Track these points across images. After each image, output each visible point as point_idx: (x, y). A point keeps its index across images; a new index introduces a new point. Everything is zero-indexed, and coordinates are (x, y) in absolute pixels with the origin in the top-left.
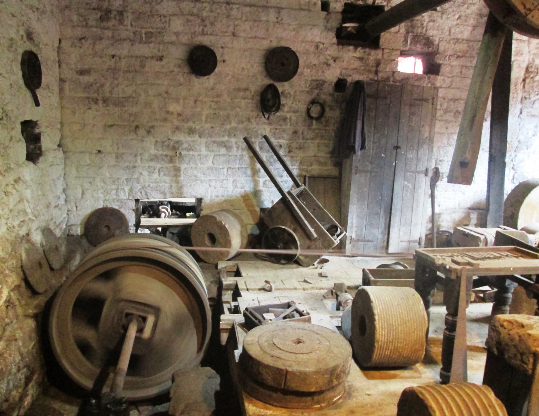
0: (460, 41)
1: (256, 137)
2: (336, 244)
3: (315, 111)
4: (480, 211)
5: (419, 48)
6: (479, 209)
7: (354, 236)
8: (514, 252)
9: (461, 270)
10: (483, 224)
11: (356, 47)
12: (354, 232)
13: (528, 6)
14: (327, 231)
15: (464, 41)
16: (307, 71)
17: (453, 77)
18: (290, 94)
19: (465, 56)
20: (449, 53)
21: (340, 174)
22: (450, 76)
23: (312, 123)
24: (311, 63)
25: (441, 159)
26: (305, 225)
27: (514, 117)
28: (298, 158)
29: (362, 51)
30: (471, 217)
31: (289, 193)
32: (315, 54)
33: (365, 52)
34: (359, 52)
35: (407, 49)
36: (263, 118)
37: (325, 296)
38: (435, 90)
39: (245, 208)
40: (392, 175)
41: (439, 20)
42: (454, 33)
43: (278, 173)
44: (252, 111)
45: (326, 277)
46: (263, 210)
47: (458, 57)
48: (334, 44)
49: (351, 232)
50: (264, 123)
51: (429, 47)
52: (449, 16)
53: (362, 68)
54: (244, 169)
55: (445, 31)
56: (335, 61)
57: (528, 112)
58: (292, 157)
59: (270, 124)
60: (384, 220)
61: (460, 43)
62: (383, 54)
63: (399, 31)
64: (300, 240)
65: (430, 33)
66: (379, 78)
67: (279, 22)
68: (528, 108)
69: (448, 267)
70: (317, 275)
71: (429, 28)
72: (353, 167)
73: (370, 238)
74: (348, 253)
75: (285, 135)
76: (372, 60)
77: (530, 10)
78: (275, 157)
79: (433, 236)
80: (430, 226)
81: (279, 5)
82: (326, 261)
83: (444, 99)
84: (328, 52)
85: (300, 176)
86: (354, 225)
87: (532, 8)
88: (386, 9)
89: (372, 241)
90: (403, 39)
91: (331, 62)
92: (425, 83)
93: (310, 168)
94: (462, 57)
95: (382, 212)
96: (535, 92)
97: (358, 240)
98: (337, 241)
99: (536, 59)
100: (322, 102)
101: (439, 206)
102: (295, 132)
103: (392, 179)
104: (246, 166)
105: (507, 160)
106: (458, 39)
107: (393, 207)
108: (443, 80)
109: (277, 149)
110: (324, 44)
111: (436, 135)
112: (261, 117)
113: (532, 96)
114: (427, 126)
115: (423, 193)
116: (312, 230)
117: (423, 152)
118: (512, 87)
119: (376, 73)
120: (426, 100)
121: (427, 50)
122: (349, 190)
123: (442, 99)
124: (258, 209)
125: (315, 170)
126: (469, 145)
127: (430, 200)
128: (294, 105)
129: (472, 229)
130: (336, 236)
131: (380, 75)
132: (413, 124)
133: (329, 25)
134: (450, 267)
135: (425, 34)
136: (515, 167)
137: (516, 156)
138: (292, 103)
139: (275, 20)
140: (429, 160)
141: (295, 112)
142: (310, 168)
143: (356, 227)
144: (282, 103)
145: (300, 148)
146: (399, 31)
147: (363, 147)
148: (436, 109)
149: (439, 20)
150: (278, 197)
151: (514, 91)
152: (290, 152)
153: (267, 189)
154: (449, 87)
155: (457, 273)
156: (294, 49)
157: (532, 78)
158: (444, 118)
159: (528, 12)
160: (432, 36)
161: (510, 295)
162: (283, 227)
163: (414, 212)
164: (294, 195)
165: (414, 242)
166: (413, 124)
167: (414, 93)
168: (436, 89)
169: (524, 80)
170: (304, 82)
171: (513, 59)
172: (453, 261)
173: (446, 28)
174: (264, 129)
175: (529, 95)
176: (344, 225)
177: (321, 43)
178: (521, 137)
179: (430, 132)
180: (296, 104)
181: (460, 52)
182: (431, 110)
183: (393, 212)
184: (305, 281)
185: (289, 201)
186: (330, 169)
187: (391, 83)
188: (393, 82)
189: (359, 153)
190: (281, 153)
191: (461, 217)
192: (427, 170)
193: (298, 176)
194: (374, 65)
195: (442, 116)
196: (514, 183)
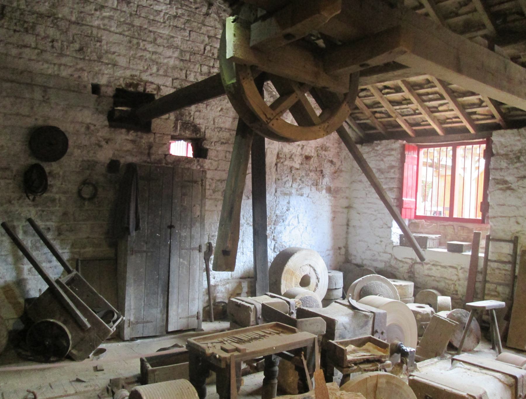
0: (223, 129)
1: (19, 219)
2: (113, 332)
3: (87, 192)
4: (249, 279)
5: (188, 134)
6: (249, 278)
7: (132, 319)
8: (276, 328)
9: (230, 358)
10: (253, 293)
11: (128, 131)
12: (132, 315)
13: (268, 116)
14: (101, 318)
15: (227, 130)
16: (77, 152)
17: (219, 160)
18: (58, 174)
19: (228, 143)
20: (215, 140)
21: (116, 255)
22: (216, 159)
23: (84, 204)
24: (81, 143)
25: (213, 234)
26: (76, 314)
27: (271, 195)
28: (70, 241)
29: (135, 134)
30: (243, 286)
31: (57, 281)
32: (86, 135)
33: (137, 135)
34: (132, 135)
35: (177, 134)
36: (27, 200)
37: (100, 395)
38: (204, 173)
39: (6, 301)
40: (168, 254)
41: (204, 110)
42: (218, 123)
43: (47, 258)
44: (13, 192)
45: (103, 370)
46: (29, 301)
47: (222, 143)
48: (106, 126)
49: (129, 316)
50: (28, 204)
51: (196, 134)
52: (213, 108)
53: (135, 150)
54: (3, 257)
55: (209, 120)
56: (107, 143)
57: (281, 191)
58: (62, 240)
59: (35, 206)
60: (162, 300)
61: (223, 131)
62: (154, 138)
63: (169, 118)
64: (71, 333)
65: (197, 121)
66: (152, 160)
67: (46, 100)
68: (280, 187)
69: (217, 356)
70: (92, 369)
71: (195, 117)
72: (129, 248)
73: (149, 319)
74: (126, 337)
75: (54, 217)
76: (144, 143)
77: (270, 119)
78: (42, 242)
79: (210, 309)
80: (207, 298)
81: (45, 84)
82: (103, 351)
83: (212, 180)
84: (100, 134)
85: (71, 259)
86: (132, 308)
87: (272, 118)
88: (157, 97)
89: (152, 322)
90: (173, 125)
91: (103, 143)
92: (195, 167)
93: (82, 251)
94: (226, 143)
95: (160, 292)
96: (285, 174)
97: (137, 323)
98: (113, 329)
99: (284, 148)
100: (94, 183)
101: (214, 278)
102: (65, 214)
103: (168, 257)
104: (6, 253)
105: (268, 232)
106: (221, 128)
107: (170, 285)
108: (211, 163)
109: (44, 232)
110: (95, 126)
111: (207, 213)
112: (25, 199)
113: (283, 177)
114: (197, 205)
115: (198, 269)
116: (85, 320)
117: (196, 230)
118: (267, 170)
119: (149, 155)
120: (196, 182)
121: (195, 137)
122: (125, 272)
123: (210, 180)
124: (22, 301)
125: (89, 251)
126: (230, 235)
127: (205, 273)
128: (63, 186)
129: (245, 300)
130: (112, 323)
131: (153, 157)
132: (185, 204)
133: (100, 108)
134: (219, 356)
135: (193, 122)
136: (275, 238)
137: (275, 228)
138: (62, 184)
139: (42, 99)
140: (202, 236)
141: (64, 193)
142: (82, 251)
143: (134, 309)
144: (49, 183)
145: (71, 230)
146: (169, 118)
147: (137, 228)
148: (205, 189)
149: (204, 110)
150: (45, 287)
151: (269, 174)
152: (59, 234)
153: (33, 277)
154: (216, 170)
155: (226, 362)
156: (63, 129)
157: (282, 163)
158: (213, 197)
159: (269, 121)
160: (199, 124)
161: (277, 368)
162: (52, 320)
163: (191, 287)
164: (64, 283)
165: (192, 317)
166: (185, 204)
167: (185, 175)
168: (204, 172)
169: (276, 165)
170: (74, 163)
171: (266, 146)
172: (223, 349)
173: (211, 118)
174: (29, 211)
175: (281, 177)
176: (122, 310)
177: (92, 124)
178: (278, 212)
179: (201, 211)
180: (66, 185)
181: (224, 139)
182: (201, 191)
183: (170, 290)
184: (78, 380)
185: (58, 291)
186: (105, 251)
187: (164, 165)
188: (166, 164)
189: (134, 234)
190: (49, 236)
191: (234, 287)
192: (200, 246)
193: (68, 261)
194: (147, 147)
195: (211, 195)
196: (275, 252)
